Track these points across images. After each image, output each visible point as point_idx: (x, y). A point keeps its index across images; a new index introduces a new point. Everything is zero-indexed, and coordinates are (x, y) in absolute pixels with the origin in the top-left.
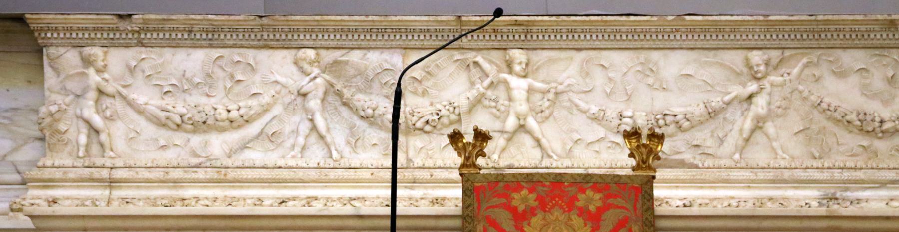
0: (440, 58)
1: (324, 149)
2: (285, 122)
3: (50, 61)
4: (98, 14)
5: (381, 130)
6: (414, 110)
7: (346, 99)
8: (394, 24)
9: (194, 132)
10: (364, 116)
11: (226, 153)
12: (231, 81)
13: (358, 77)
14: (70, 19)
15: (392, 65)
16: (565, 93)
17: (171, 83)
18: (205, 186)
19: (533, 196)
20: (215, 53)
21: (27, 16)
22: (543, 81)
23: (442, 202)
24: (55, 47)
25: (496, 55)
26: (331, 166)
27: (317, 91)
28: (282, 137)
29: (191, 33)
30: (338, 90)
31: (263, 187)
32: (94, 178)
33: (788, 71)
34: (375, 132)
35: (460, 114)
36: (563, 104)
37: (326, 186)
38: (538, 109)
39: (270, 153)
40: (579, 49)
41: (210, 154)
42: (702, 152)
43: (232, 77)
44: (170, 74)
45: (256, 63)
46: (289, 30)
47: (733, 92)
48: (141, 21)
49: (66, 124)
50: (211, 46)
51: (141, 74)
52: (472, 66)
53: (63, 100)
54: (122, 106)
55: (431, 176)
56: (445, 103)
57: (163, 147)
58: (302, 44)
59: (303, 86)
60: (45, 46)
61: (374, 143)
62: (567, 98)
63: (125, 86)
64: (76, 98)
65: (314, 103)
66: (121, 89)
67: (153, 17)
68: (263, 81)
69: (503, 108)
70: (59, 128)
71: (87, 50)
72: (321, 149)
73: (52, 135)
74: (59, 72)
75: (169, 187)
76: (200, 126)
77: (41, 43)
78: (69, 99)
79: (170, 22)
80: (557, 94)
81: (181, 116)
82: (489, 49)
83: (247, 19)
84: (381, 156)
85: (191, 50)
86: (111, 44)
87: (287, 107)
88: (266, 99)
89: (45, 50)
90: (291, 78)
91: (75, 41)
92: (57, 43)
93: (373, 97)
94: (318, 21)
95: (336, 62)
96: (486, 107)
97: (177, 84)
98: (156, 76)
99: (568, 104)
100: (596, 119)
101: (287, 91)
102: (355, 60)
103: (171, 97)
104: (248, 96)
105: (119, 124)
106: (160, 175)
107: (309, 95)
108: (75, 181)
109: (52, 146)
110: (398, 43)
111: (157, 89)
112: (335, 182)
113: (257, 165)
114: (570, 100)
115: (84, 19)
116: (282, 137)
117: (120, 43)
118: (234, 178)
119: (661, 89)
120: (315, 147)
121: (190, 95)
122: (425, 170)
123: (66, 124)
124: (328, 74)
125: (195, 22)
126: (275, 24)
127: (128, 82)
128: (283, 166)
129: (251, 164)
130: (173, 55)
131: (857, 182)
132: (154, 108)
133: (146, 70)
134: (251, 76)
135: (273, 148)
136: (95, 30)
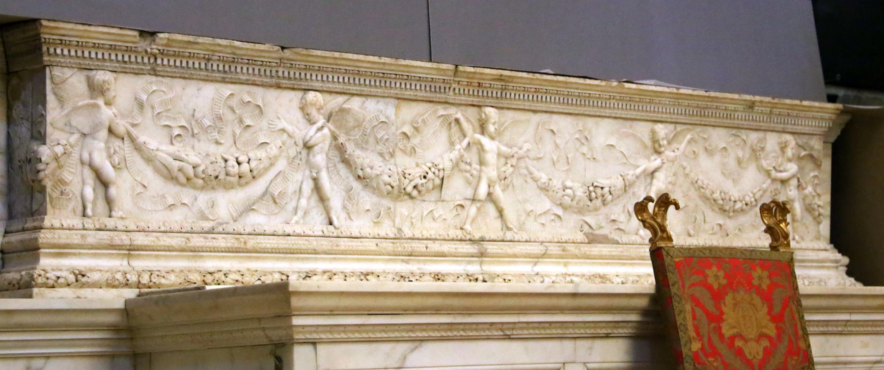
0: (427, 112)
1: (322, 214)
2: (289, 180)
3: (54, 86)
5: (374, 193)
6: (405, 171)
8: (402, 69)
9: (202, 188)
10: (362, 176)
12: (240, 126)
14: (90, 31)
15: (387, 117)
16: (523, 159)
17: (181, 124)
18: (223, 257)
19: (721, 274)
20: (227, 90)
21: (44, 23)
25: (472, 112)
26: (335, 235)
27: (324, 143)
30: (342, 144)
31: (278, 259)
33: (677, 147)
34: (368, 196)
39: (273, 217)
40: (535, 112)
42: (617, 227)
43: (241, 121)
45: (264, 106)
47: (641, 165)
48: (165, 42)
49: (69, 172)
50: (223, 81)
52: (453, 124)
53: (67, 141)
55: (427, 248)
57: (171, 207)
58: (311, 86)
59: (311, 137)
60: (48, 66)
61: (367, 208)
63: (134, 125)
65: (319, 159)
67: (179, 37)
68: (269, 127)
69: (475, 172)
70: (63, 177)
71: (101, 76)
73: (54, 186)
75: (188, 257)
78: (73, 139)
81: (194, 167)
83: (271, 50)
84: (372, 224)
86: (123, 69)
87: (292, 161)
88: (273, 150)
94: (336, 58)
95: (342, 110)
97: (187, 126)
98: (164, 114)
99: (525, 172)
100: (545, 189)
101: (293, 141)
104: (255, 146)
107: (316, 149)
111: (166, 131)
112: (343, 254)
113: (267, 232)
114: (527, 168)
115: (104, 33)
118: (254, 247)
119: (592, 159)
121: (199, 141)
123: (69, 172)
124: (332, 124)
129: (262, 232)
130: (184, 89)
131: (344, 252)
133: (156, 106)
134: (259, 121)
135: (277, 211)
136: (112, 48)
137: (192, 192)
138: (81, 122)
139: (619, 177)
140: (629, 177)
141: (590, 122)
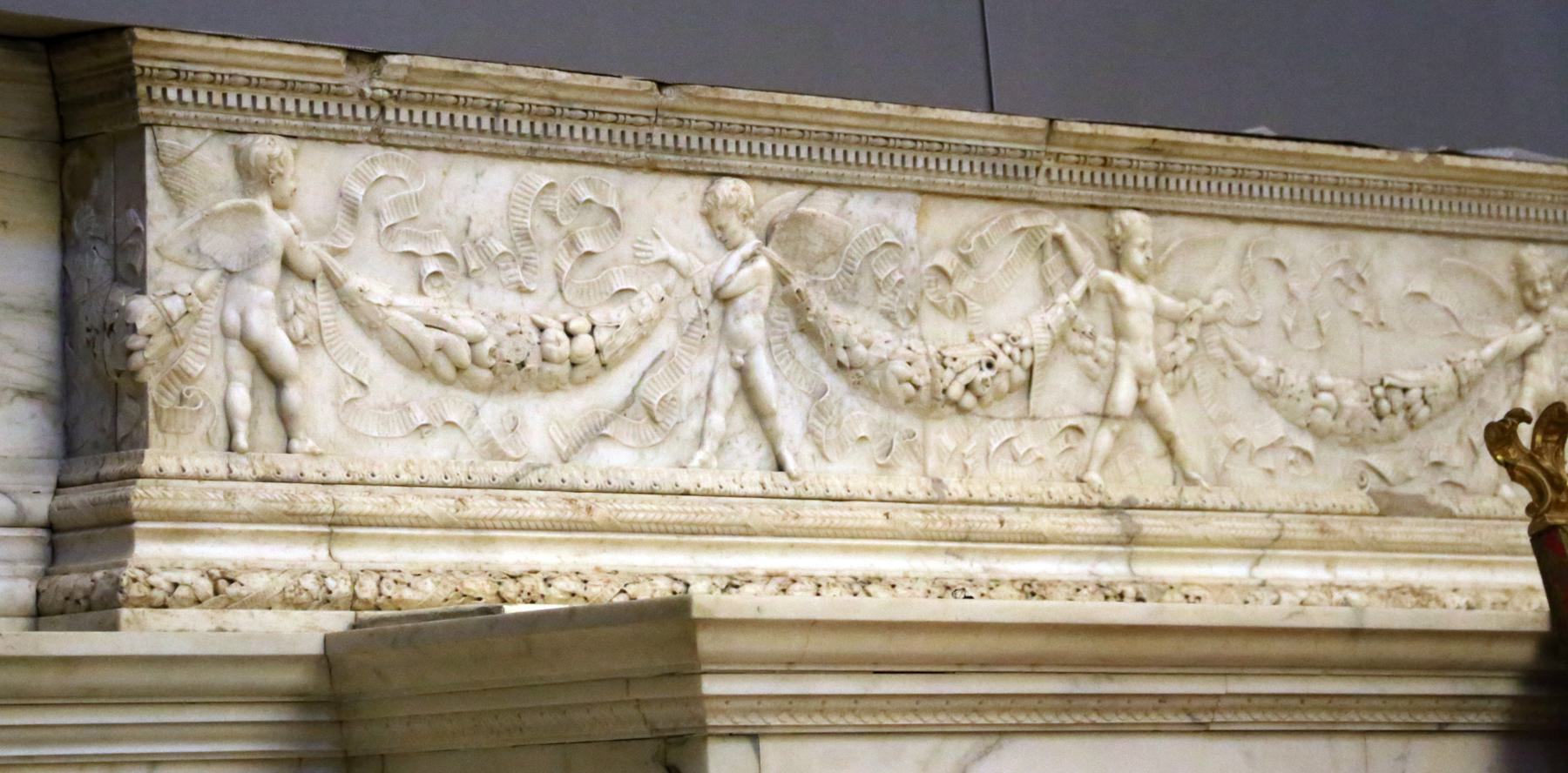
2: (683, 372)
3: (162, 169)
4: (306, 45)
6: (944, 352)
7: (815, 317)
11: (557, 448)
13: (831, 259)
16: (1213, 327)
17: (438, 251)
20: (540, 175)
21: (141, 34)
22: (1174, 294)
23: (1043, 592)
24: (174, 129)
28: (676, 411)
29: (498, 116)
30: (798, 291)
31: (664, 546)
32: (299, 511)
35: (1031, 369)
36: (1211, 352)
37: (792, 546)
38: (1169, 362)
39: (649, 454)
40: (1236, 220)
41: (524, 451)
42: (1445, 479)
43: (572, 243)
44: (439, 226)
45: (623, 210)
46: (711, 126)
47: (1496, 339)
48: (401, 73)
50: (532, 156)
51: (372, 220)
52: (1049, 247)
54: (329, 310)
55: (1002, 523)
56: (999, 338)
58: (726, 166)
60: (150, 125)
61: (863, 434)
62: (1216, 338)
63: (337, 253)
64: (224, 280)
66: (330, 260)
67: (432, 63)
68: (635, 257)
70: (184, 365)
71: (263, 147)
72: (754, 447)
74: (182, 200)
75: (462, 542)
76: (510, 374)
77: (147, 115)
78: (205, 281)
79: (468, 82)
80: (1204, 325)
81: (470, 344)
82: (1076, 206)
83: (636, 88)
85: (483, 163)
86: (311, 132)
88: (645, 306)
89: (148, 133)
90: (696, 255)
91: (229, 117)
92: (186, 118)
93: (859, 312)
94: (779, 106)
95: (797, 220)
96: (1073, 351)
97: (453, 253)
99: (1219, 352)
100: (1268, 392)
102: (828, 215)
103: (439, 288)
105: (320, 359)
106: (448, 506)
107: (741, 301)
108: (250, 518)
109: (165, 417)
110: (916, 178)
111: (406, 264)
114: (1224, 344)
115: (271, 55)
116: (676, 411)
117: (334, 130)
119: (1376, 326)
120: (743, 439)
121: (481, 286)
122: (971, 507)
125: (519, 87)
126: (688, 105)
127: (342, 241)
128: (692, 491)
132: (408, 318)
133: (385, 211)
134: (612, 244)
136: (286, 86)
137: (468, 397)
138: (222, 244)
139: (1444, 364)
140: (1468, 366)
141: (1368, 242)
